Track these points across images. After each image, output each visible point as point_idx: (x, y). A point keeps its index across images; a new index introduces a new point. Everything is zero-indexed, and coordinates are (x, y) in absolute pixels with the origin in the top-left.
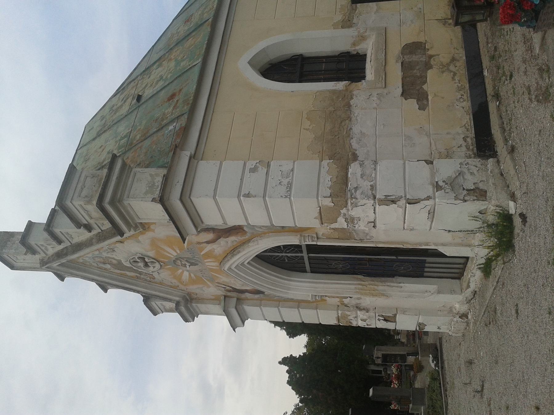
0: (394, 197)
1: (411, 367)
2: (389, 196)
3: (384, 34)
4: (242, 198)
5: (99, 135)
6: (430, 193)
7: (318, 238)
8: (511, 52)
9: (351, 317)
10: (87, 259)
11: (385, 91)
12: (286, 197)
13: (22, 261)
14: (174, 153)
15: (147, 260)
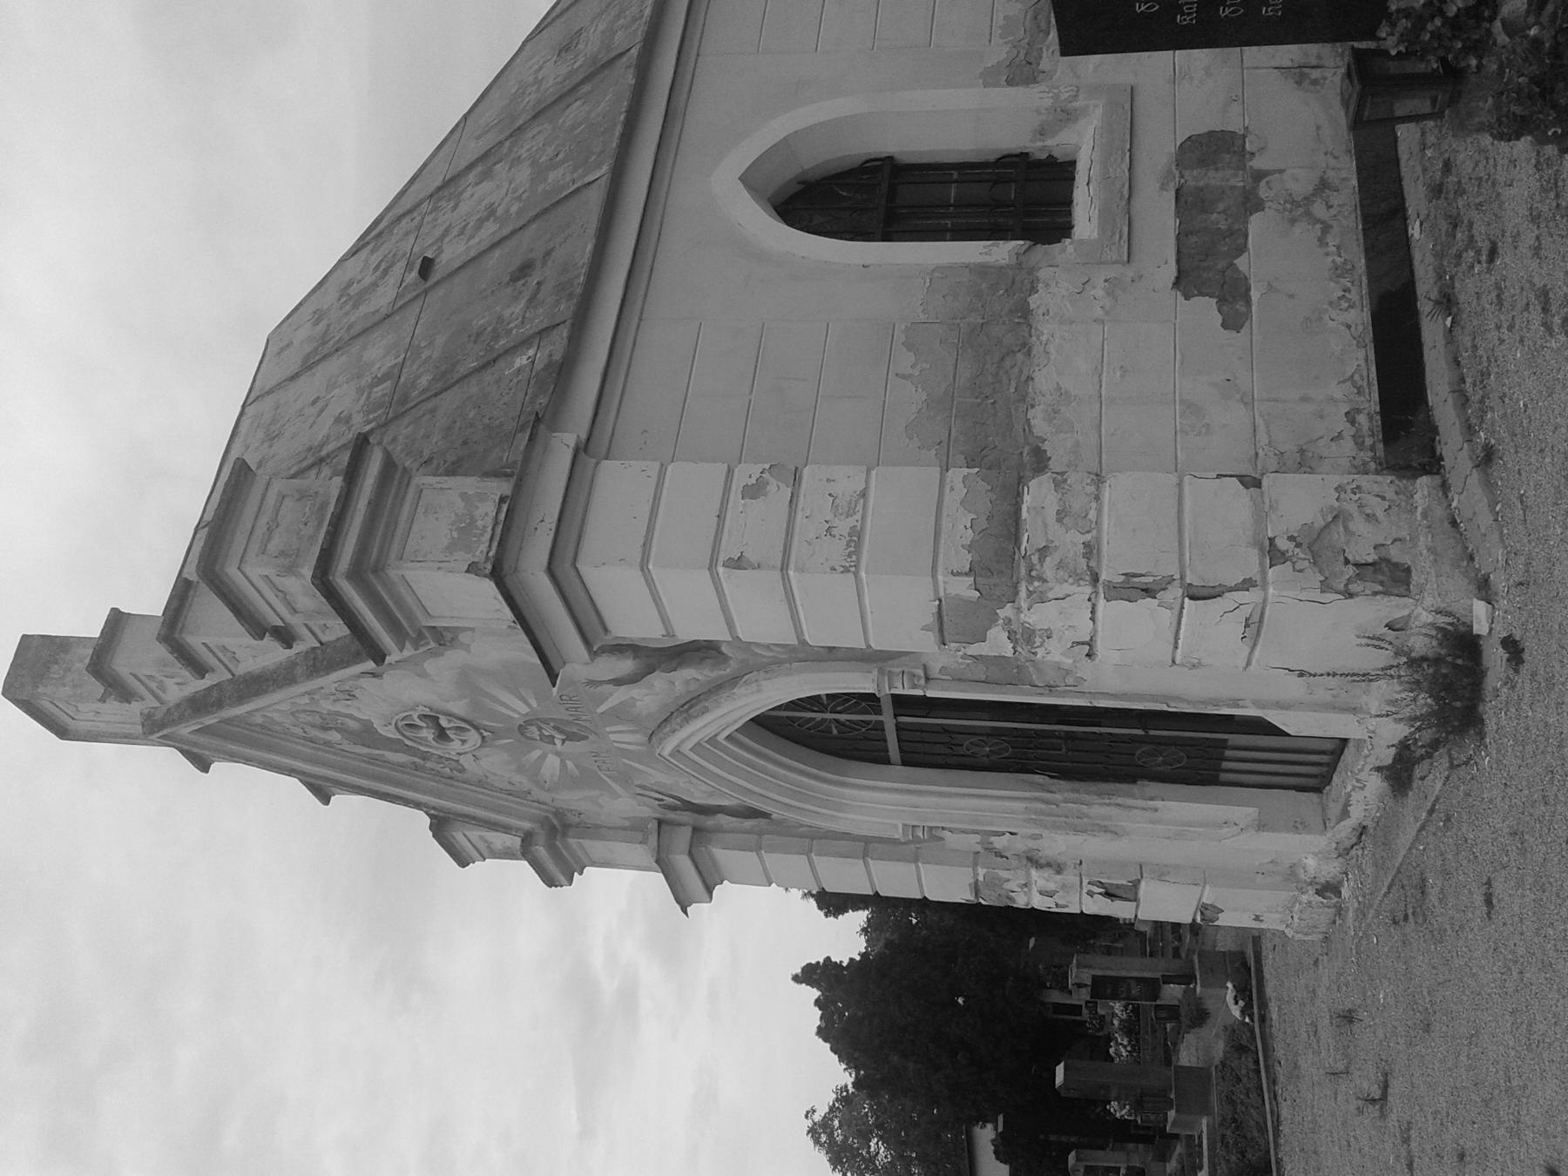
0: (1151, 579)
1: (1173, 1012)
2: (1135, 575)
3: (1128, 107)
4: (721, 570)
5: (308, 366)
6: (1253, 571)
7: (927, 679)
8: (1494, 184)
9: (1011, 886)
10: (275, 716)
11: (1130, 272)
12: (846, 570)
13: (91, 716)
14: (530, 439)
15: (444, 722)
